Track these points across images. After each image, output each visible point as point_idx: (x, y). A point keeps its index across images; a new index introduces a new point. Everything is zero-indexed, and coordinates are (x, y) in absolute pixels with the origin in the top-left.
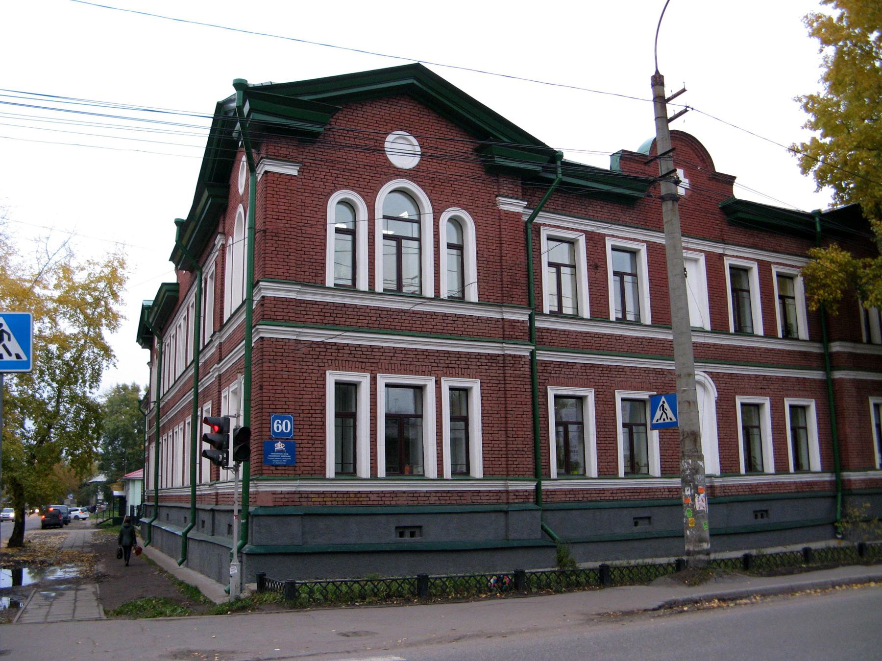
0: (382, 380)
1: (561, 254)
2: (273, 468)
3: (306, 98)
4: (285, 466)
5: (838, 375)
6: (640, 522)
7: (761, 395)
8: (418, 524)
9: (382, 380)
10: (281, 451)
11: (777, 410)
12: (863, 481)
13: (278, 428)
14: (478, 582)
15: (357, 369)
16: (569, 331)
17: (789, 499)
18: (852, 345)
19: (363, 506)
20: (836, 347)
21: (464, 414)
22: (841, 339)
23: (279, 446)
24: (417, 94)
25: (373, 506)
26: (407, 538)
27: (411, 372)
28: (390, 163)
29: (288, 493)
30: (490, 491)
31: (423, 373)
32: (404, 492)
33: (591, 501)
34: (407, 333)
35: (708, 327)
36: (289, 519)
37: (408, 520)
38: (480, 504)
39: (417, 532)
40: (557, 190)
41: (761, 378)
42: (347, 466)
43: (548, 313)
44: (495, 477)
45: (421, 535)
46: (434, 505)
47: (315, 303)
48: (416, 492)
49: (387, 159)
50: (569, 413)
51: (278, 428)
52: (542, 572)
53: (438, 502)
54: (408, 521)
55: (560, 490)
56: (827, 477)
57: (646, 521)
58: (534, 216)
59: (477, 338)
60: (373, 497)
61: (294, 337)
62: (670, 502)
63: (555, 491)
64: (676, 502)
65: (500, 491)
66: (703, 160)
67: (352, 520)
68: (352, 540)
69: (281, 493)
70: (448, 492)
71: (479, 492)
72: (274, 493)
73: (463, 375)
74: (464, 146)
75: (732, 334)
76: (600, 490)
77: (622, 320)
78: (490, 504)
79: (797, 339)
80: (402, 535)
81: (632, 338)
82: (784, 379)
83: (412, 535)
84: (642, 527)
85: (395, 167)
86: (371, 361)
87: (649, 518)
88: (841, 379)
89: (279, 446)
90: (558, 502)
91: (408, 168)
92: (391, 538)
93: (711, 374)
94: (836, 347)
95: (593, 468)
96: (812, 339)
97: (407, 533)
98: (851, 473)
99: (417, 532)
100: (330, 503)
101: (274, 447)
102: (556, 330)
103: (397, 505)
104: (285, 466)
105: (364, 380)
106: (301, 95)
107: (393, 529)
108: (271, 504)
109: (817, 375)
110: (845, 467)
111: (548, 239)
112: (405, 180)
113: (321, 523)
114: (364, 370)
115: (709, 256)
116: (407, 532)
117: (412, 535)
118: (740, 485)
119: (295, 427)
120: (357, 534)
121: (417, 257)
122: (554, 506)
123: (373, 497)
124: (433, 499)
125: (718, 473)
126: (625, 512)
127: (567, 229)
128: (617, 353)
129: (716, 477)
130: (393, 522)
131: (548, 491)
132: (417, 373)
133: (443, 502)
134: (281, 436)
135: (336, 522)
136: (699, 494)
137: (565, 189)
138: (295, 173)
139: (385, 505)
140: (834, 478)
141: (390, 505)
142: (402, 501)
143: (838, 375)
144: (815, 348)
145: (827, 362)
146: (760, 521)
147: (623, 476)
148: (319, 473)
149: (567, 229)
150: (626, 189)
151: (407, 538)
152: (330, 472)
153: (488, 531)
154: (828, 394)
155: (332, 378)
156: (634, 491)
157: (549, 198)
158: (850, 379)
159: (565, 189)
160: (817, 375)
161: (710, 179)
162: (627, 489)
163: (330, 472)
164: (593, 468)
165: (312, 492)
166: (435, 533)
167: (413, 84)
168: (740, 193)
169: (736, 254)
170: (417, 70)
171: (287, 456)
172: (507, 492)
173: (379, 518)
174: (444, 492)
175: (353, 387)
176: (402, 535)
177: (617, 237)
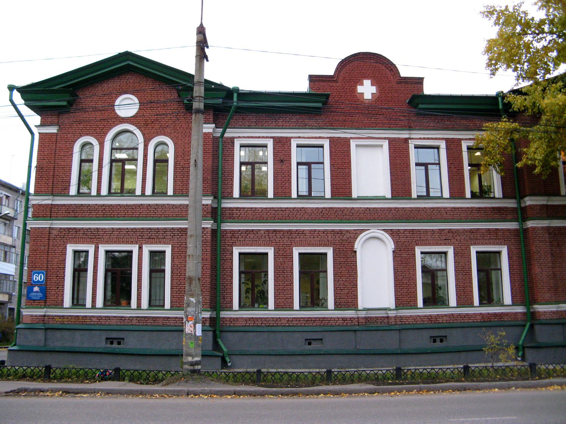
0: (146, 249)
1: (428, 156)
2: (32, 301)
3: (56, 88)
4: (39, 300)
5: (530, 224)
6: (313, 342)
7: (445, 244)
8: (122, 337)
9: (102, 249)
10: (37, 292)
11: (462, 258)
12: (553, 312)
13: (36, 279)
14: (444, 372)
15: (88, 243)
16: (256, 208)
17: (426, 328)
18: (546, 198)
19: (87, 324)
20: (529, 201)
21: (499, 267)
22: (534, 194)
23: (36, 289)
24: (126, 69)
25: (94, 325)
26: (115, 345)
27: (123, 243)
28: (118, 115)
29: (40, 316)
30: (176, 318)
31: (132, 243)
32: (115, 317)
33: (268, 326)
34: (122, 218)
35: (389, 195)
36: (35, 331)
37: (114, 336)
38: (168, 326)
39: (444, 339)
40: (236, 112)
41: (447, 231)
42: (78, 301)
43: (416, 197)
44: (341, 309)
45: (123, 344)
46: (136, 325)
47: (64, 205)
48: (123, 317)
49: (116, 114)
50: (434, 263)
51: (36, 279)
52: (285, 372)
53: (138, 324)
54: (114, 335)
55: (242, 318)
56: (520, 309)
57: (319, 342)
58: (224, 132)
59: (172, 218)
60: (94, 319)
61: (49, 226)
62: (342, 328)
63: (237, 318)
64: (179, 328)
65: (383, 317)
66: (392, 70)
67: (77, 333)
68: (86, 345)
69: (36, 316)
70: (146, 317)
71: (168, 318)
72: (32, 316)
73: (160, 243)
74: (168, 94)
75: (271, 199)
76: (277, 319)
77: (300, 197)
78: (176, 326)
79: (494, 198)
80: (435, 341)
81: (312, 209)
82: (471, 231)
83: (119, 343)
84: (315, 346)
85: (120, 117)
86: (95, 237)
87: (321, 339)
88: (534, 228)
89: (36, 289)
90: (240, 326)
91: (129, 116)
92: (101, 344)
93: (392, 233)
94: (529, 201)
95: (453, 301)
96: (506, 196)
97: (438, 340)
98: (538, 306)
99: (444, 339)
100: (66, 322)
101: (33, 289)
102: (244, 208)
103: (109, 325)
104: (39, 300)
105: (91, 248)
106: (52, 86)
107: (104, 340)
108: (29, 322)
109: (513, 225)
110: (534, 301)
111: (415, 148)
112: (126, 124)
113: (58, 334)
114: (92, 243)
115: (392, 141)
116: (115, 342)
117: (441, 341)
118: (418, 316)
119: (46, 278)
120: (79, 341)
121: (438, 171)
122: (234, 329)
123: (94, 319)
124: (134, 322)
125: (393, 306)
126: (297, 335)
127: (259, 137)
128: (323, 221)
129: (390, 310)
130: (104, 335)
131: (224, 318)
132: (127, 243)
133: (141, 324)
134: (38, 283)
135: (67, 333)
136: (188, 322)
137: (240, 110)
138: (55, 131)
139: (101, 325)
140: (525, 311)
141: (105, 325)
142: (113, 322)
143: (530, 224)
144: (511, 204)
145: (523, 214)
146: (438, 344)
147: (298, 308)
148: (59, 304)
149: (259, 137)
150: (323, 103)
151: (115, 345)
152: (168, 305)
153: (390, 341)
154: (521, 242)
155: (70, 249)
156: (430, 317)
157: (231, 118)
158: (543, 228)
159: (240, 110)
160: (513, 225)
161: (399, 83)
162: (302, 318)
163: (168, 305)
164: (453, 301)
165: (56, 316)
166: (132, 342)
167: (129, 65)
168: (429, 89)
169: (422, 136)
170: (127, 55)
171: (40, 295)
172: (388, 317)
173: (94, 332)
174: (143, 317)
175: (498, 254)
176: (435, 341)
177: (304, 138)
